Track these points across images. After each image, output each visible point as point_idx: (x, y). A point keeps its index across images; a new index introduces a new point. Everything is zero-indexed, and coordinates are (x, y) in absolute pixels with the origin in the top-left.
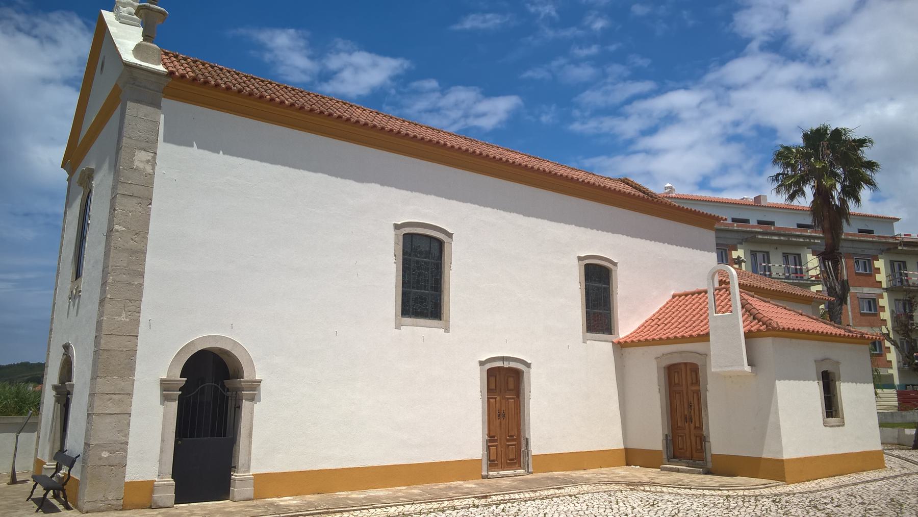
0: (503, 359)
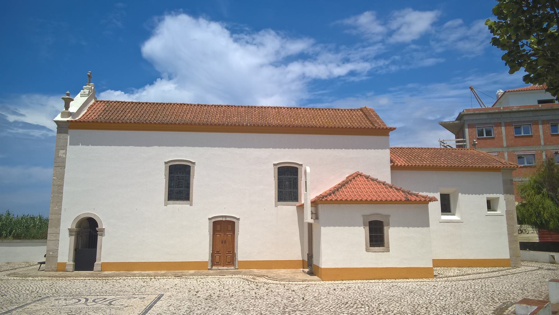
0: (226, 217)
